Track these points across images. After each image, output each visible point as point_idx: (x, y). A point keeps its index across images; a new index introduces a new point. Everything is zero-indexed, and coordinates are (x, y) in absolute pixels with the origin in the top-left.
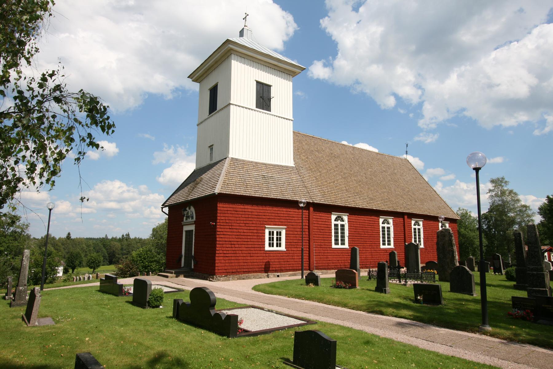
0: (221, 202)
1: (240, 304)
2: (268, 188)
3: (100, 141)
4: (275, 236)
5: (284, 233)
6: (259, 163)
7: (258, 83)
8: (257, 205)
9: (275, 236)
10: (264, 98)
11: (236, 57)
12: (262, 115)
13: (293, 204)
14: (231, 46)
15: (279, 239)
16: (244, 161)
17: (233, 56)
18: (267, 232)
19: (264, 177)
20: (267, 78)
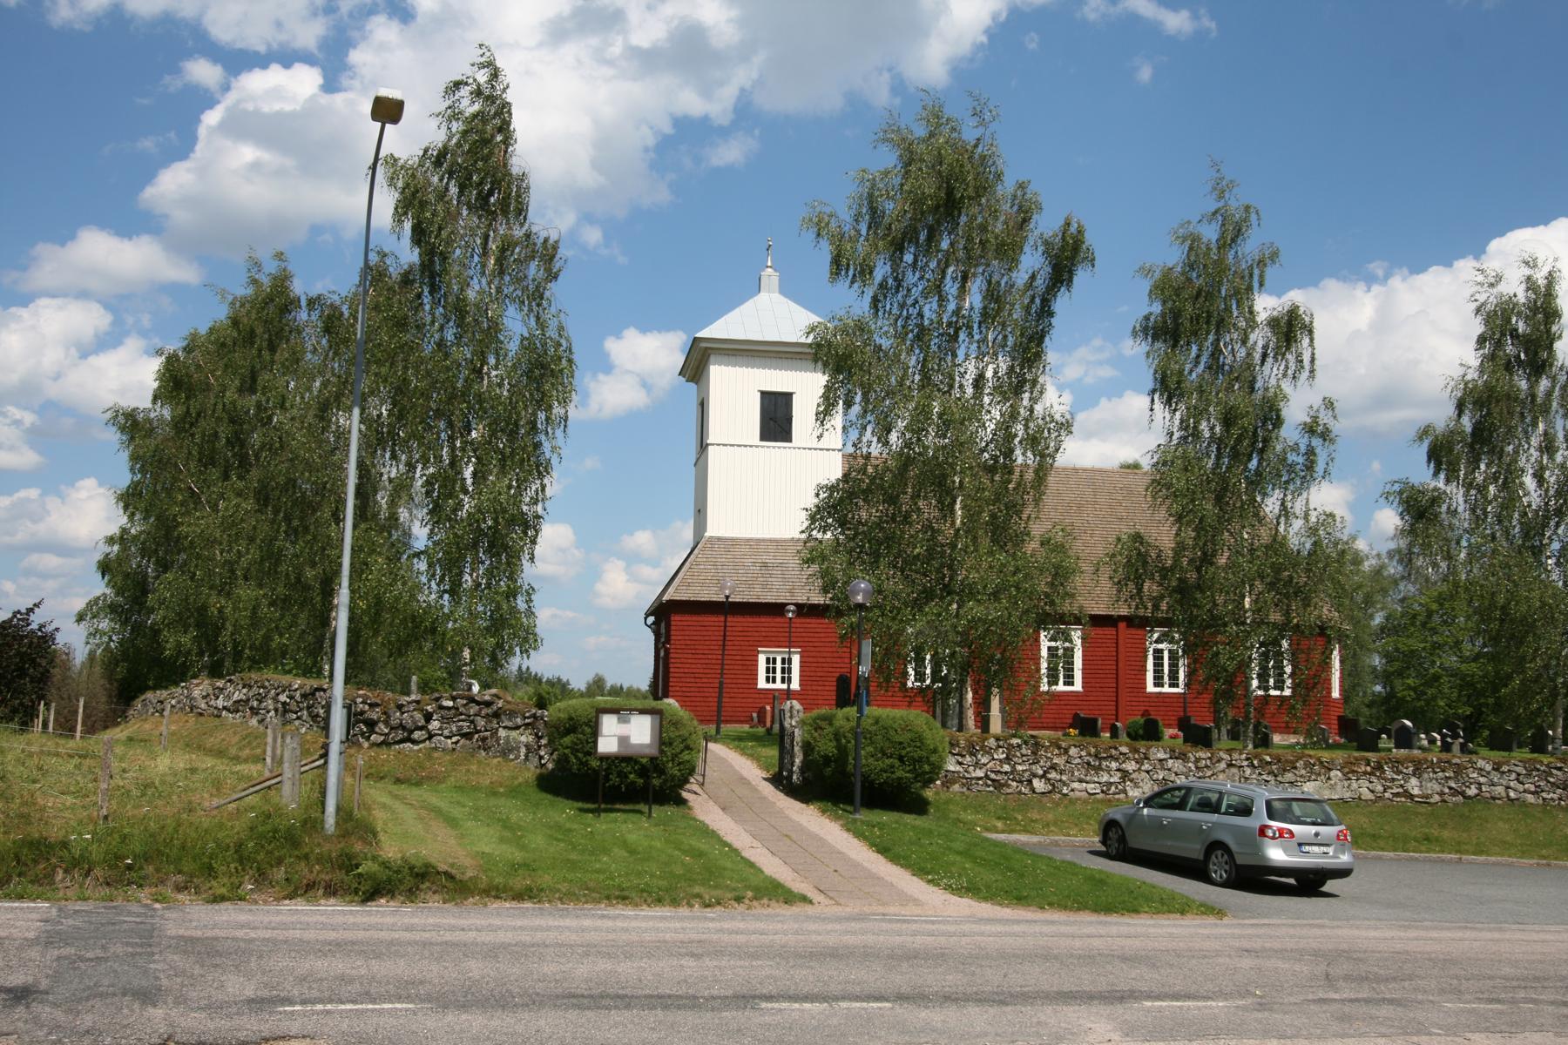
0: (676, 613)
1: (837, 818)
2: (764, 586)
3: (1310, 280)
4: (779, 666)
5: (796, 659)
6: (764, 540)
7: (763, 393)
8: (743, 614)
9: (779, 666)
10: (776, 418)
11: (719, 358)
12: (775, 449)
13: (777, 609)
14: (704, 345)
15: (787, 671)
16: (733, 539)
17: (712, 358)
18: (762, 659)
19: (765, 565)
20: (778, 379)
